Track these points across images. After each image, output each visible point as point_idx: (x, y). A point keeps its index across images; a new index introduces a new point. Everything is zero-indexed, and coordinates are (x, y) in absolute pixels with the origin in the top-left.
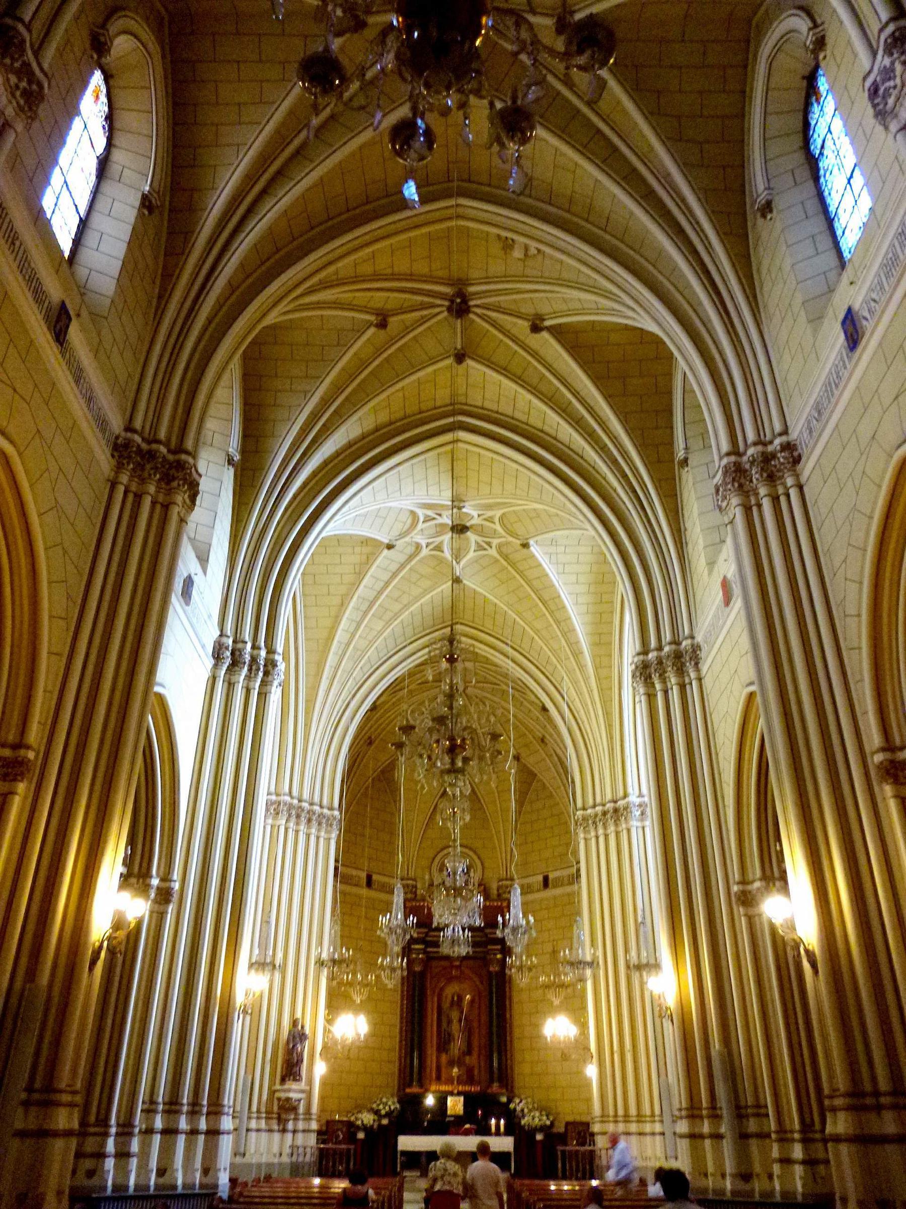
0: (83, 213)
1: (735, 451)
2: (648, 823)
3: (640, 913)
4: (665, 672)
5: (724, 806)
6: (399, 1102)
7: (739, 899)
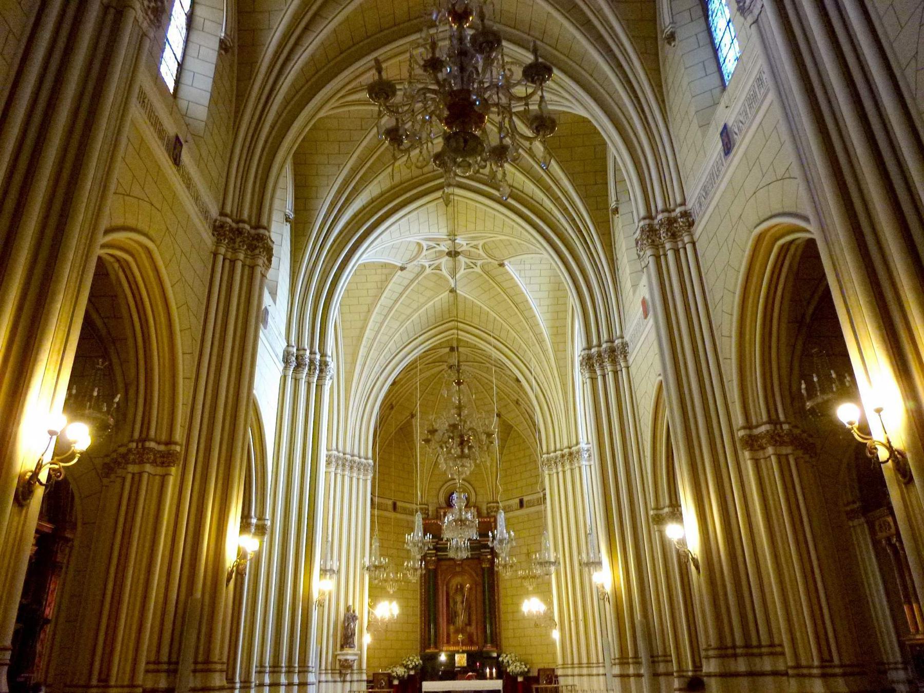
0: (179, 59)
1: (649, 217)
2: (592, 463)
3: (588, 528)
4: (603, 362)
5: (644, 456)
6: (421, 659)
7: (654, 520)
